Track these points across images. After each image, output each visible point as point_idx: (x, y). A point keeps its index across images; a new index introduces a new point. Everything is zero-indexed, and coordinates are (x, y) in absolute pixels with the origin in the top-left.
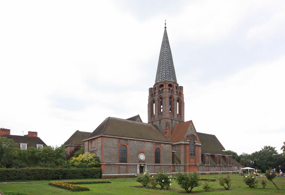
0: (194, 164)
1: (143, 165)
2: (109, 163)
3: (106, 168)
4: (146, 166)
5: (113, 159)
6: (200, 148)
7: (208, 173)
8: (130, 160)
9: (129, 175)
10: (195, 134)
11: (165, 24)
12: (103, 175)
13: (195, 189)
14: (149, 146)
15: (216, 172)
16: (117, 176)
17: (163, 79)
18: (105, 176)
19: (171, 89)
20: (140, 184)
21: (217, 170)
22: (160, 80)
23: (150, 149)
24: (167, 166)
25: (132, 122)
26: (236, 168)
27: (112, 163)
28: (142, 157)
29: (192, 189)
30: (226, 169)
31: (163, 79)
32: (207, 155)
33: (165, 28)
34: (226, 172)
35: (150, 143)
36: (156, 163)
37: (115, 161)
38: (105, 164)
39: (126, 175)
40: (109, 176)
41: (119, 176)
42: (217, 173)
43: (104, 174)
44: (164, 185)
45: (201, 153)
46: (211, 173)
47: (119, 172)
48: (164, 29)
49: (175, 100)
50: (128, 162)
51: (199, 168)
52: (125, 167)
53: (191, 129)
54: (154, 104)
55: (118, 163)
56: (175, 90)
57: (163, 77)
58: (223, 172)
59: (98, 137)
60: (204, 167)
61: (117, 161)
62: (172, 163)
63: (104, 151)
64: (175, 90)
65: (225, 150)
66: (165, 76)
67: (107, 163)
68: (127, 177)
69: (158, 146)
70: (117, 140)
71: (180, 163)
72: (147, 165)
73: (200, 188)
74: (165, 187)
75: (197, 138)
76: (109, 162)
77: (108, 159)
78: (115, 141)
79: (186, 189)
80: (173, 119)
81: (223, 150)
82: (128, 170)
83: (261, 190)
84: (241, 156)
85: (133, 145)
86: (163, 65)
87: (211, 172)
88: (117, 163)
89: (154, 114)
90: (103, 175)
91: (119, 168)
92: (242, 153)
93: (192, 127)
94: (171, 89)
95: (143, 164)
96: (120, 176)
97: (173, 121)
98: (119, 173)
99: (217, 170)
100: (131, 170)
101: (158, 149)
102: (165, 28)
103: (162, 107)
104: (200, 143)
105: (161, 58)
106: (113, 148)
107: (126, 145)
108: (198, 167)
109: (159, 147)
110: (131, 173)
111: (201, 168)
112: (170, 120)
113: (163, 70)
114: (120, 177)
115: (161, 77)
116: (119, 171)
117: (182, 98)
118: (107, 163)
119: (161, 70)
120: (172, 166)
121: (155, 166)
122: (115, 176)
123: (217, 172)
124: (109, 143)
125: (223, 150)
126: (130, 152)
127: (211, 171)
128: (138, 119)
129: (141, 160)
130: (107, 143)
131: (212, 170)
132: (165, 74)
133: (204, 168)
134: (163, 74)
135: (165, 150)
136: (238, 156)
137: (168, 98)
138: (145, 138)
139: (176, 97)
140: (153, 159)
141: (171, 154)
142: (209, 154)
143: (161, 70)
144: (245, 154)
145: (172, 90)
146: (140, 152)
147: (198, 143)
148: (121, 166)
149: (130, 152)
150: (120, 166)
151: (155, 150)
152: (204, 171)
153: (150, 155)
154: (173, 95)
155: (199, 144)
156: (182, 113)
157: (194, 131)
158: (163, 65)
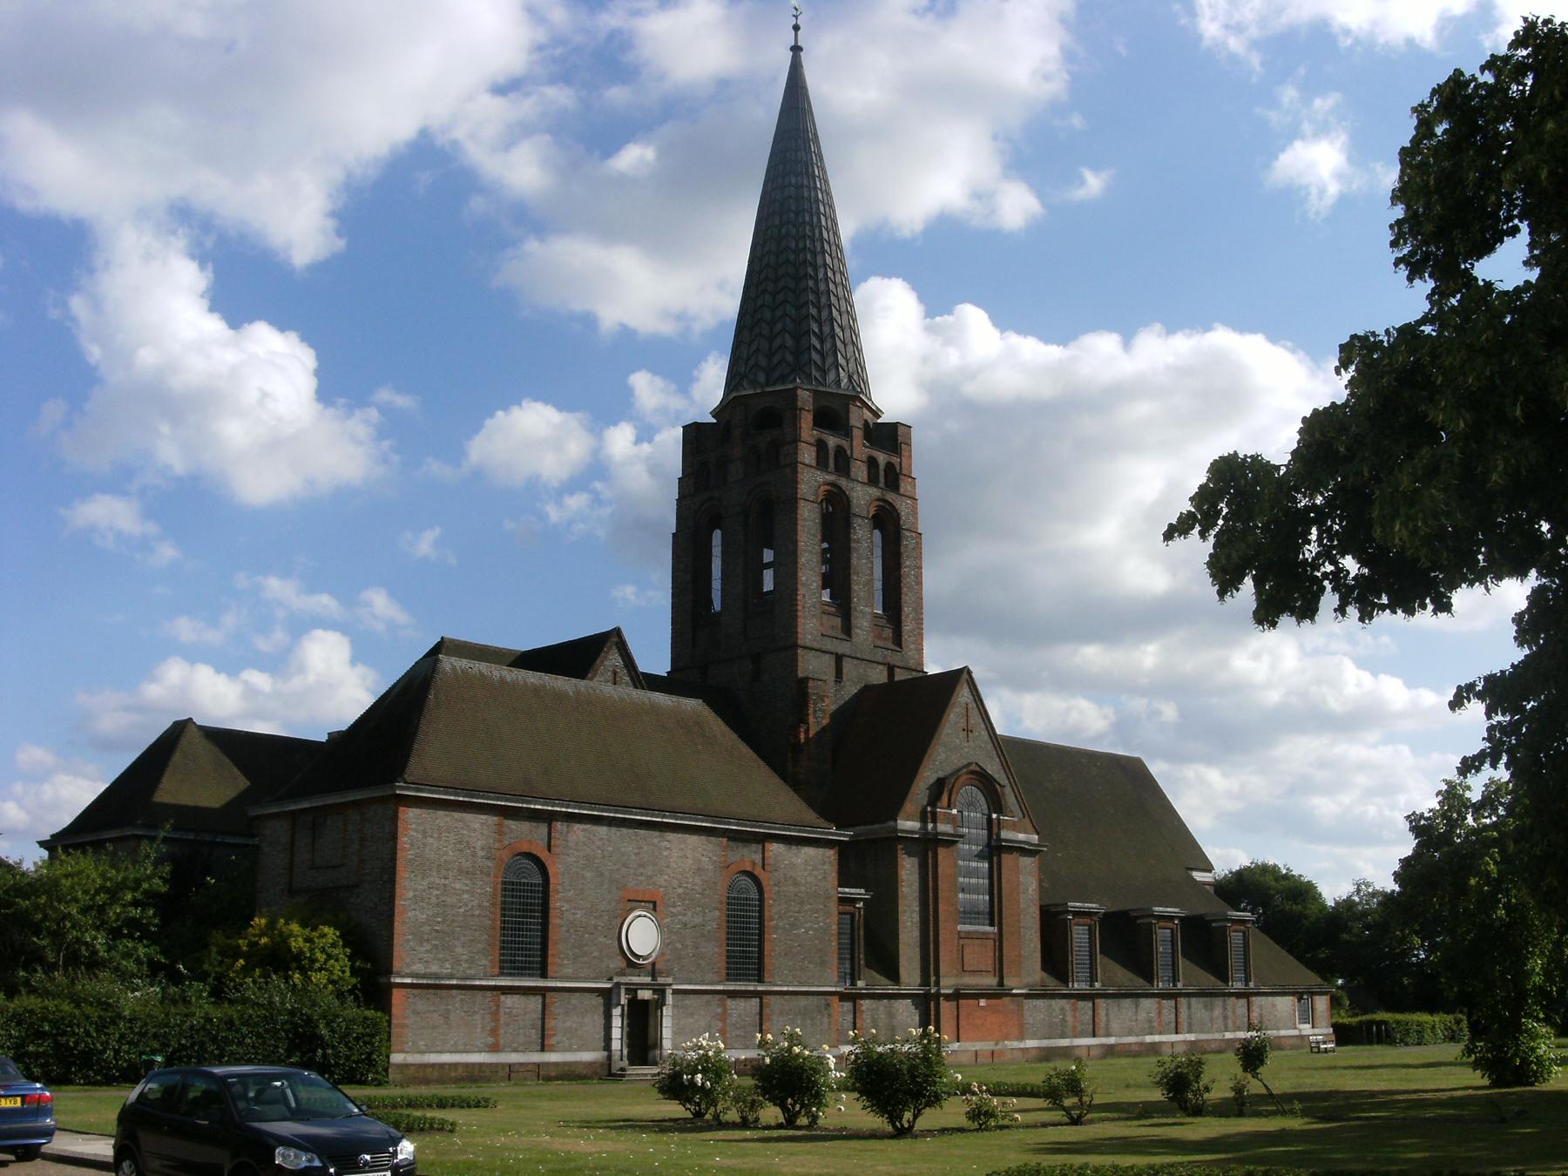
0: (990, 981)
1: (645, 995)
2: (437, 977)
3: (416, 1013)
4: (669, 998)
5: (459, 950)
6: (1027, 862)
7: (1089, 1047)
8: (567, 958)
9: (556, 1064)
10: (993, 768)
11: (796, 28)
12: (396, 1058)
13: (930, 1118)
14: (687, 860)
15: (1148, 1039)
16: (481, 1065)
17: (777, 374)
18: (407, 1066)
19: (832, 441)
20: (675, 1109)
21: (1150, 1021)
22: (762, 378)
23: (697, 880)
24: (803, 1001)
25: (578, 693)
26: (1285, 1004)
27: (451, 977)
28: (643, 936)
29: (915, 1117)
30: (1217, 1012)
31: (777, 374)
32: (1077, 914)
33: (796, 49)
34: (1218, 1036)
35: (693, 840)
36: (731, 976)
37: (471, 961)
38: (408, 981)
39: (538, 1065)
40: (433, 1065)
41: (497, 1065)
42: (1153, 1044)
43: (402, 1051)
44: (797, 1107)
45: (1036, 897)
46: (1111, 1047)
47: (491, 1040)
48: (788, 56)
49: (857, 522)
50: (550, 973)
51: (1027, 1013)
52: (535, 1003)
53: (968, 730)
54: (717, 536)
55: (493, 976)
56: (860, 449)
57: (776, 360)
58: (1192, 1037)
59: (372, 801)
60: (1063, 1002)
61: (485, 962)
62: (842, 978)
63: (411, 894)
64: (860, 449)
65: (1208, 868)
66: (790, 358)
67: (424, 976)
68: (545, 1074)
69: (748, 856)
70: (492, 820)
71: (894, 976)
72: (676, 992)
73: (953, 1112)
74: (803, 1121)
75: (1008, 790)
76: (434, 968)
77: (427, 947)
78: (479, 824)
79: (894, 1117)
80: (843, 648)
81: (1199, 876)
82: (553, 1023)
83: (766, 1011)
84: (1347, 905)
85: (583, 856)
86: (781, 284)
87: (1112, 1040)
88: (485, 977)
89: (717, 605)
90: (396, 1058)
91: (495, 1015)
92: (1352, 889)
93: (975, 718)
94: (882, 458)
95: (644, 986)
96: (503, 1065)
97: (847, 665)
98: (494, 1048)
99: (1150, 1021)
100: (568, 1024)
101: (746, 881)
102: (796, 49)
103: (768, 555)
104: (1029, 826)
105: (760, 272)
106: (460, 871)
107: (543, 855)
108: (1020, 1006)
109: (754, 864)
110: (569, 1049)
111: (1037, 1011)
112: (829, 661)
113: (779, 313)
114: (501, 1073)
115: (763, 362)
116: (494, 1032)
117: (903, 506)
118: (424, 976)
119: (768, 315)
120: (843, 997)
121: (729, 1002)
122: (466, 1065)
123: (1157, 1038)
124: (439, 839)
125: (1199, 876)
126: (569, 901)
127: (1108, 1035)
128: (613, 659)
129: (638, 957)
130: (430, 840)
131: (1115, 1026)
132: (789, 342)
133: (1062, 1009)
134: (778, 341)
135: (795, 883)
136: (1324, 907)
137: (810, 506)
138: (815, 998)
139: (862, 496)
140: (715, 952)
141: (834, 908)
142: (1092, 906)
143: (768, 315)
144: (1374, 894)
145: (840, 451)
146: (634, 902)
147: (1014, 827)
148: (509, 1001)
149: (569, 901)
150: (503, 998)
151: (730, 888)
152: (1062, 1037)
153: (698, 920)
154: (843, 482)
155: (1021, 837)
156: (906, 610)
157: (990, 746)
158: (781, 284)
